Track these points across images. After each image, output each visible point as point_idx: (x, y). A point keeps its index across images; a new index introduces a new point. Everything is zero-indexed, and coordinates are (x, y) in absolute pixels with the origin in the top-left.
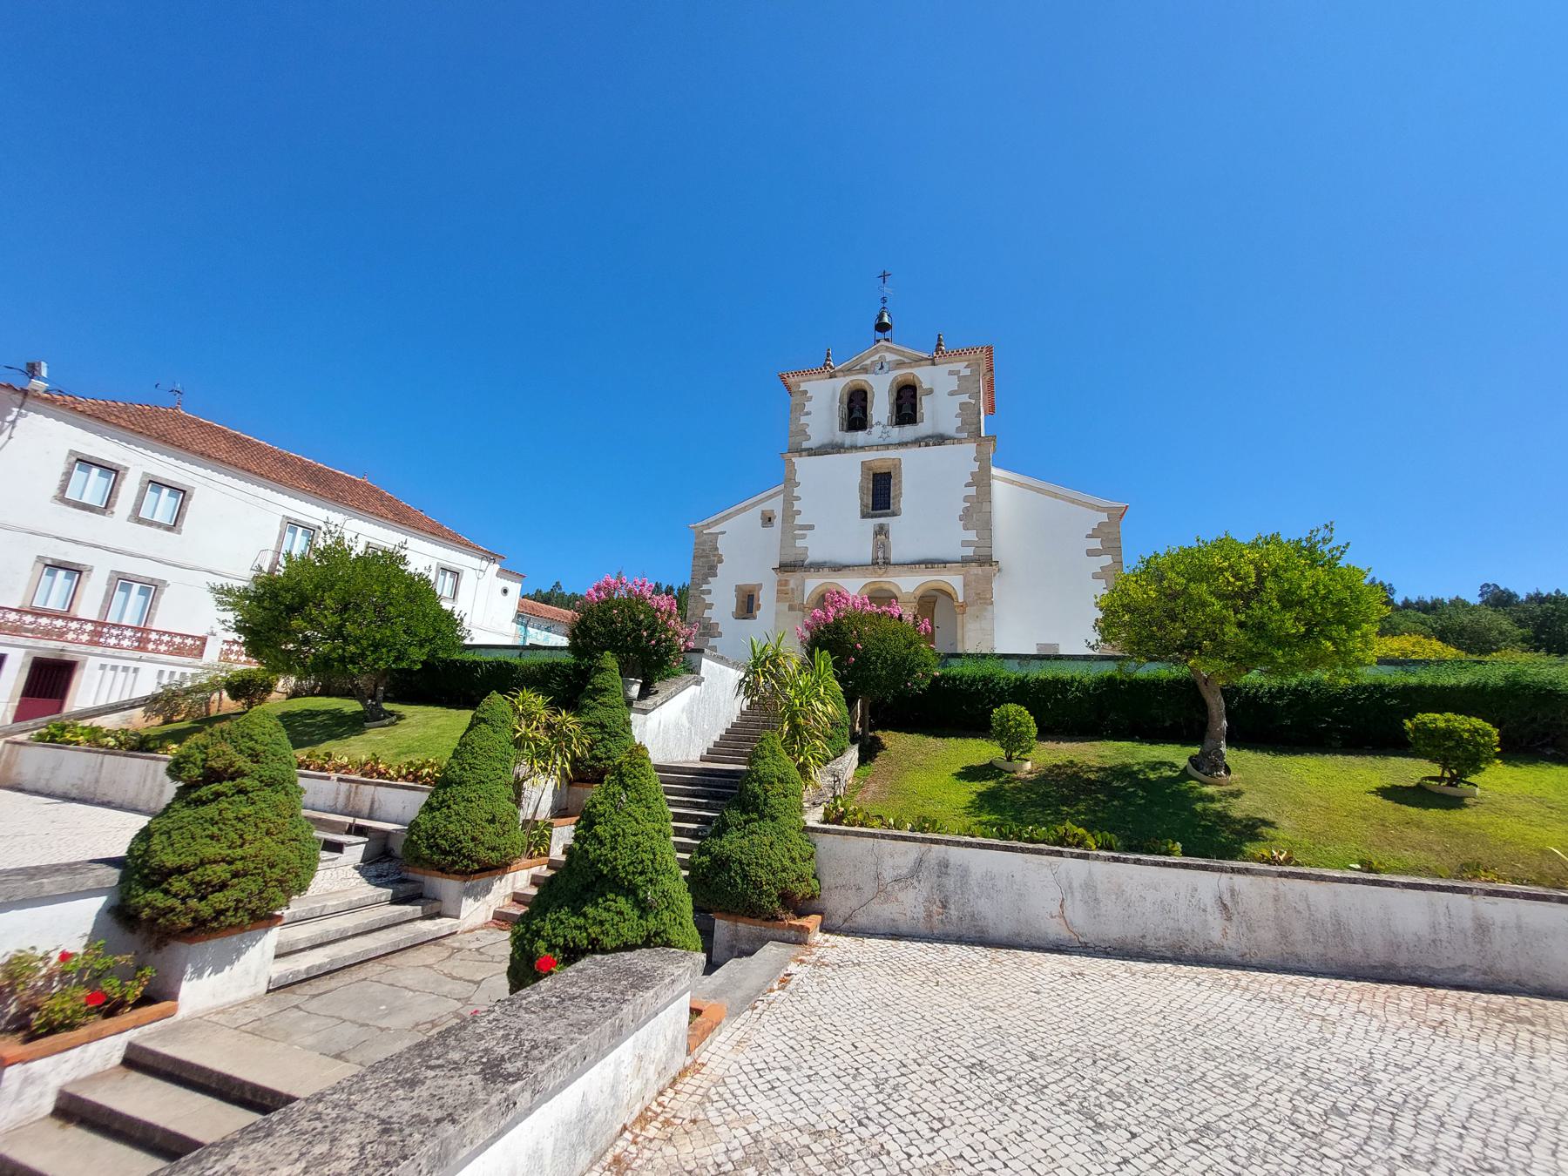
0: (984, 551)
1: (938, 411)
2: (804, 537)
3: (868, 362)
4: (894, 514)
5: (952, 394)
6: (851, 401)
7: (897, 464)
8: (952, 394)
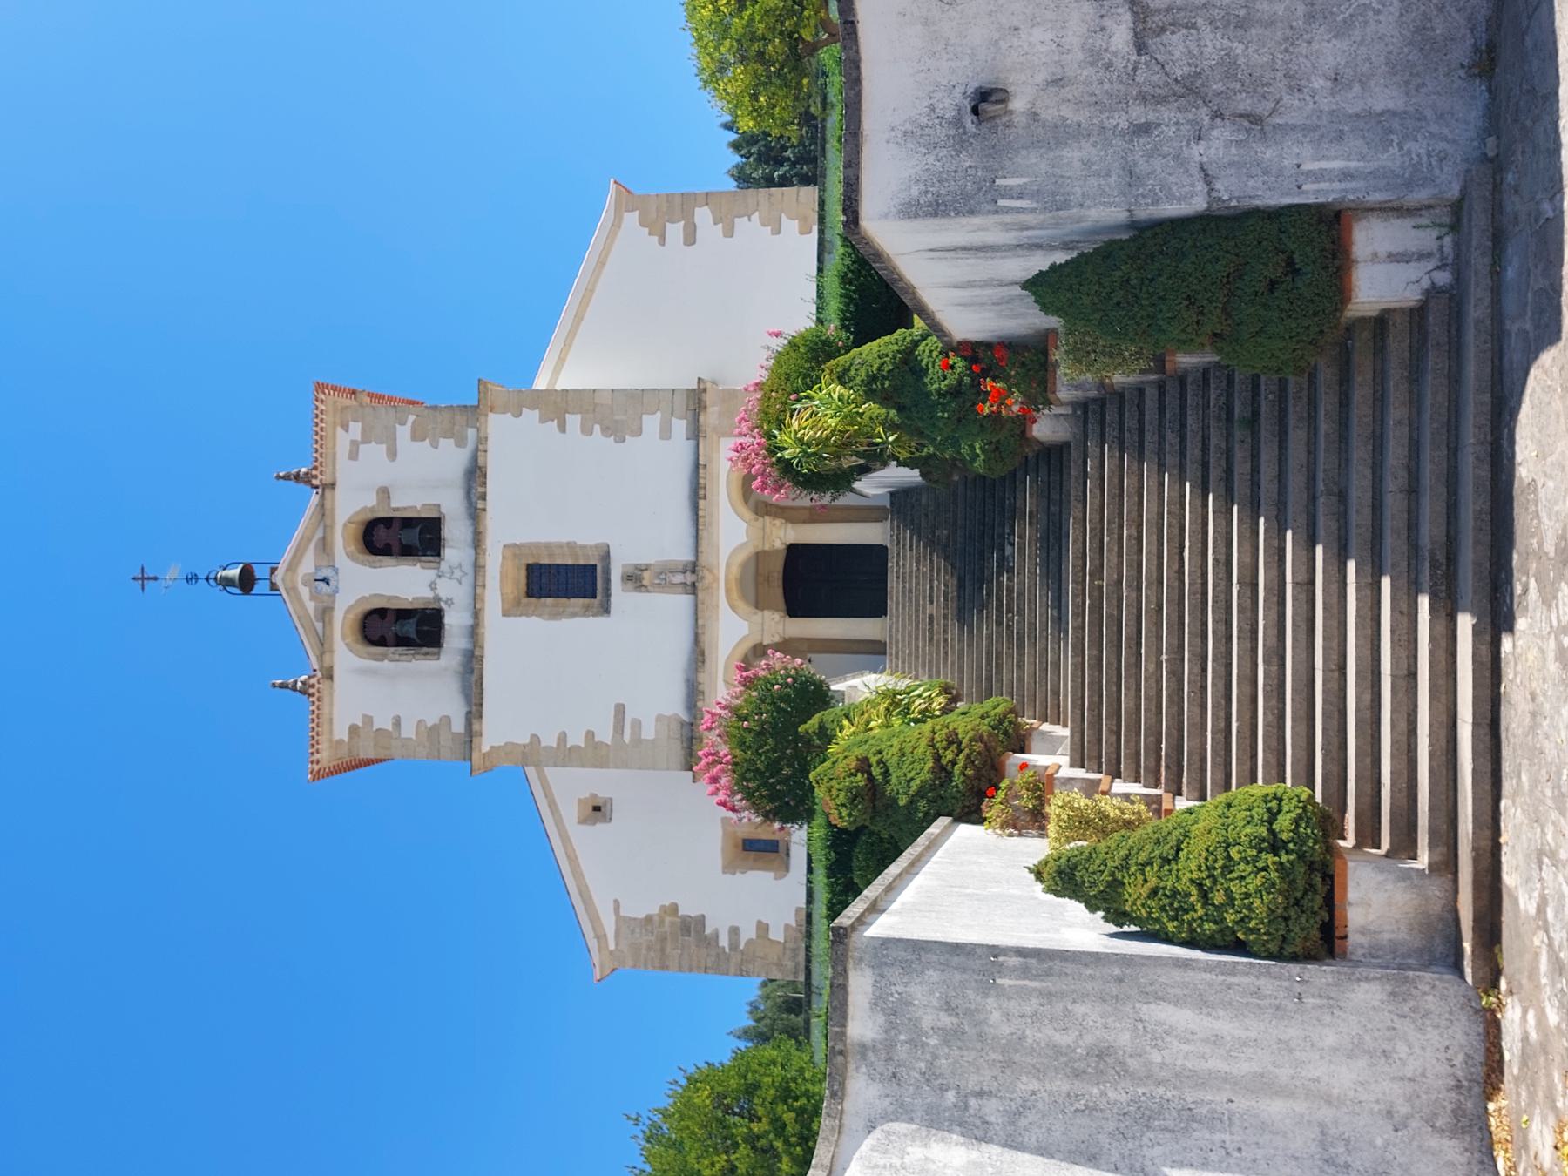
0: (681, 403)
1: (418, 477)
2: (637, 724)
3: (311, 606)
4: (606, 557)
5: (393, 454)
6: (381, 642)
7: (512, 550)
8: (393, 454)
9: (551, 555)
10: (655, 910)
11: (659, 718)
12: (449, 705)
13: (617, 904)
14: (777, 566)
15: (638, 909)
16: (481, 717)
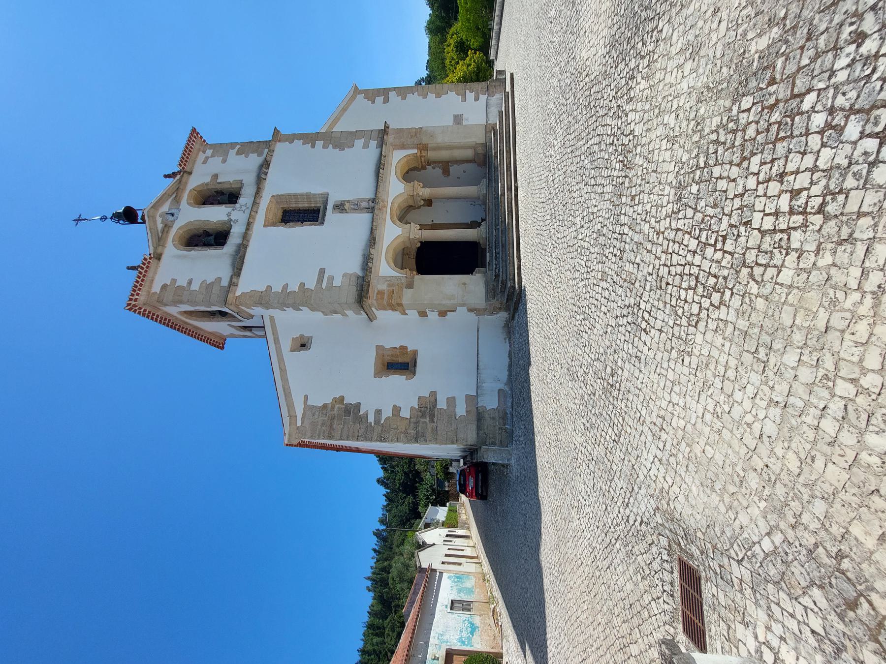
2: (331, 279)
5: (224, 161)
7: (278, 199)
9: (296, 202)
10: (329, 401)
11: (345, 275)
12: (224, 273)
13: (306, 397)
14: (413, 253)
15: (317, 401)
16: (239, 275)
